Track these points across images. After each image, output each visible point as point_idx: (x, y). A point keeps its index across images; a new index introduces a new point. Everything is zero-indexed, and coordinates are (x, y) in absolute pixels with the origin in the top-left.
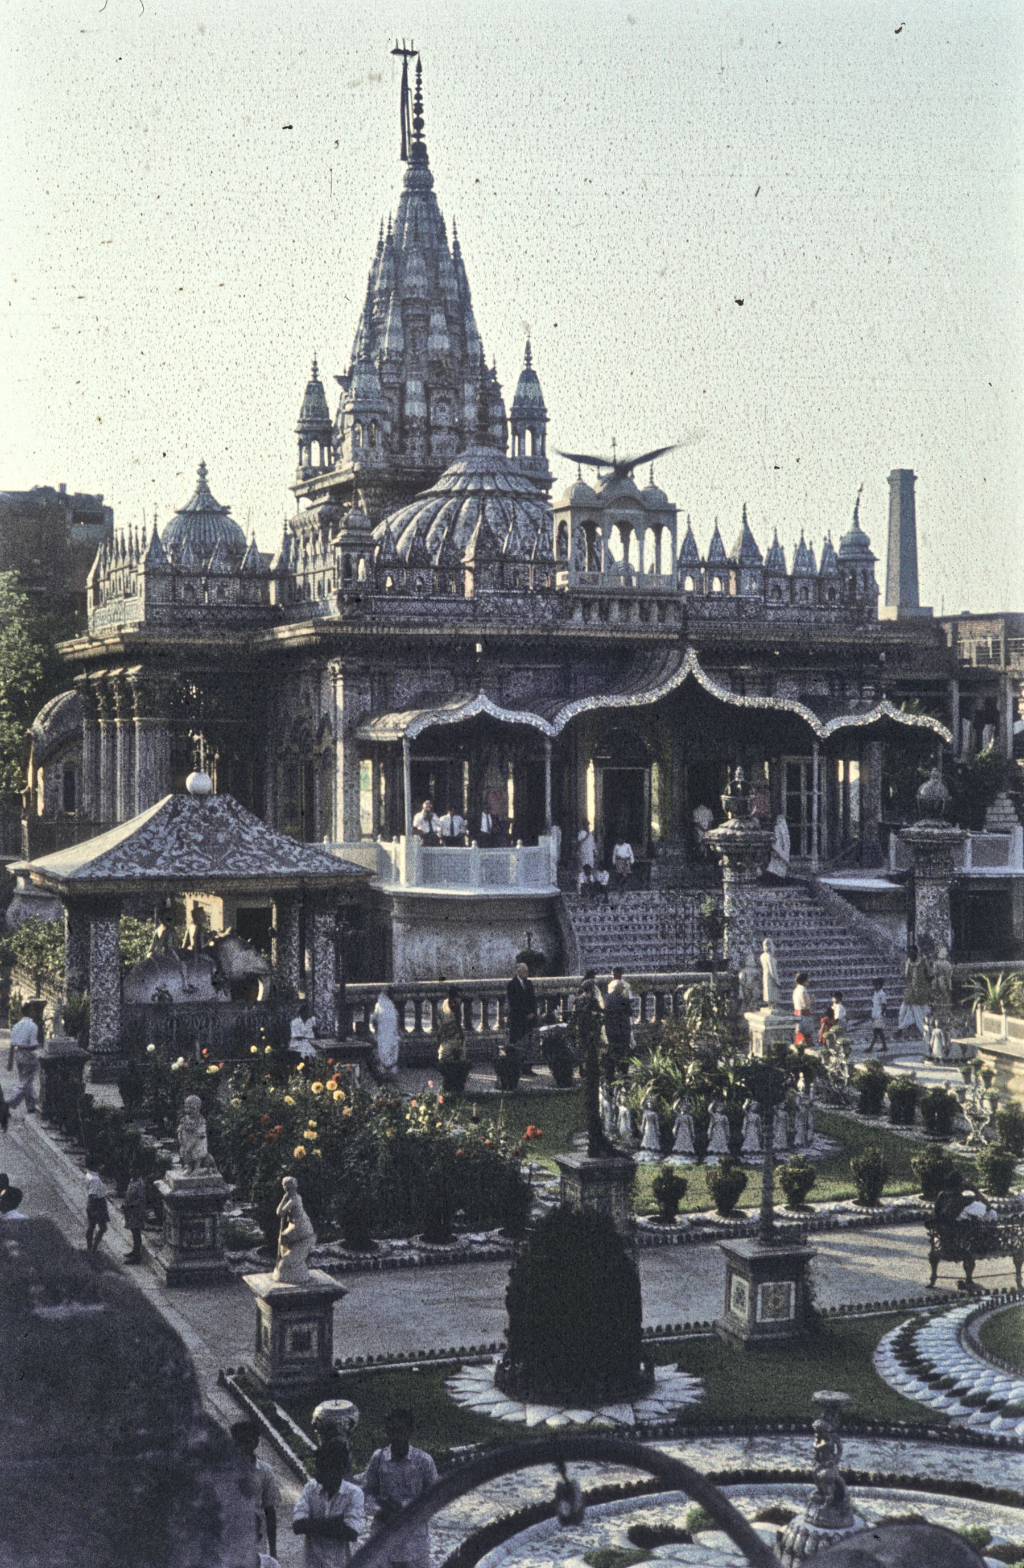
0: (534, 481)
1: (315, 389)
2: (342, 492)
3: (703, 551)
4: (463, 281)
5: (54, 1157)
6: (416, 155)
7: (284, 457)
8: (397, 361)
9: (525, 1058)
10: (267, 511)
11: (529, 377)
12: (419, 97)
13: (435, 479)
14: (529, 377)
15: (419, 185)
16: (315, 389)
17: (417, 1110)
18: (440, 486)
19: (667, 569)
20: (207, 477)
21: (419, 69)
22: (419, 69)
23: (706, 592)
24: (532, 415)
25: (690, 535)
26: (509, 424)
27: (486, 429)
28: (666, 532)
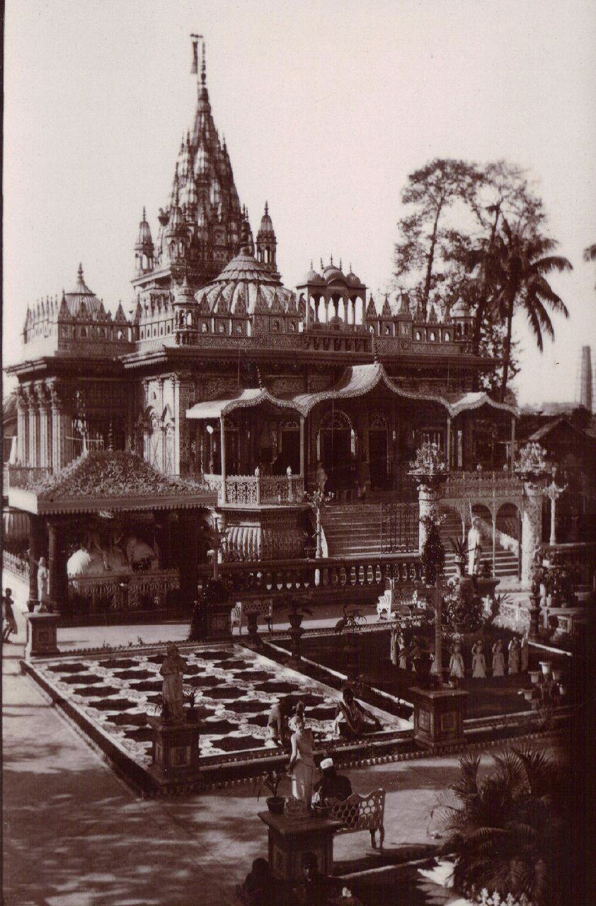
0: (273, 277)
1: (145, 224)
2: (164, 282)
3: (379, 310)
4: (229, 165)
5: (106, 842)
6: (204, 96)
7: (130, 265)
8: (193, 208)
9: (494, 228)
10: (118, 292)
11: (266, 219)
12: (204, 62)
13: (218, 273)
14: (266, 219)
15: (205, 111)
16: (145, 224)
17: (230, 232)
18: (222, 277)
19: (359, 321)
20: (83, 275)
21: (204, 46)
22: (204, 46)
23: (289, 638)
24: (268, 239)
25: (372, 299)
26: (256, 246)
27: (244, 243)
28: (359, 300)
